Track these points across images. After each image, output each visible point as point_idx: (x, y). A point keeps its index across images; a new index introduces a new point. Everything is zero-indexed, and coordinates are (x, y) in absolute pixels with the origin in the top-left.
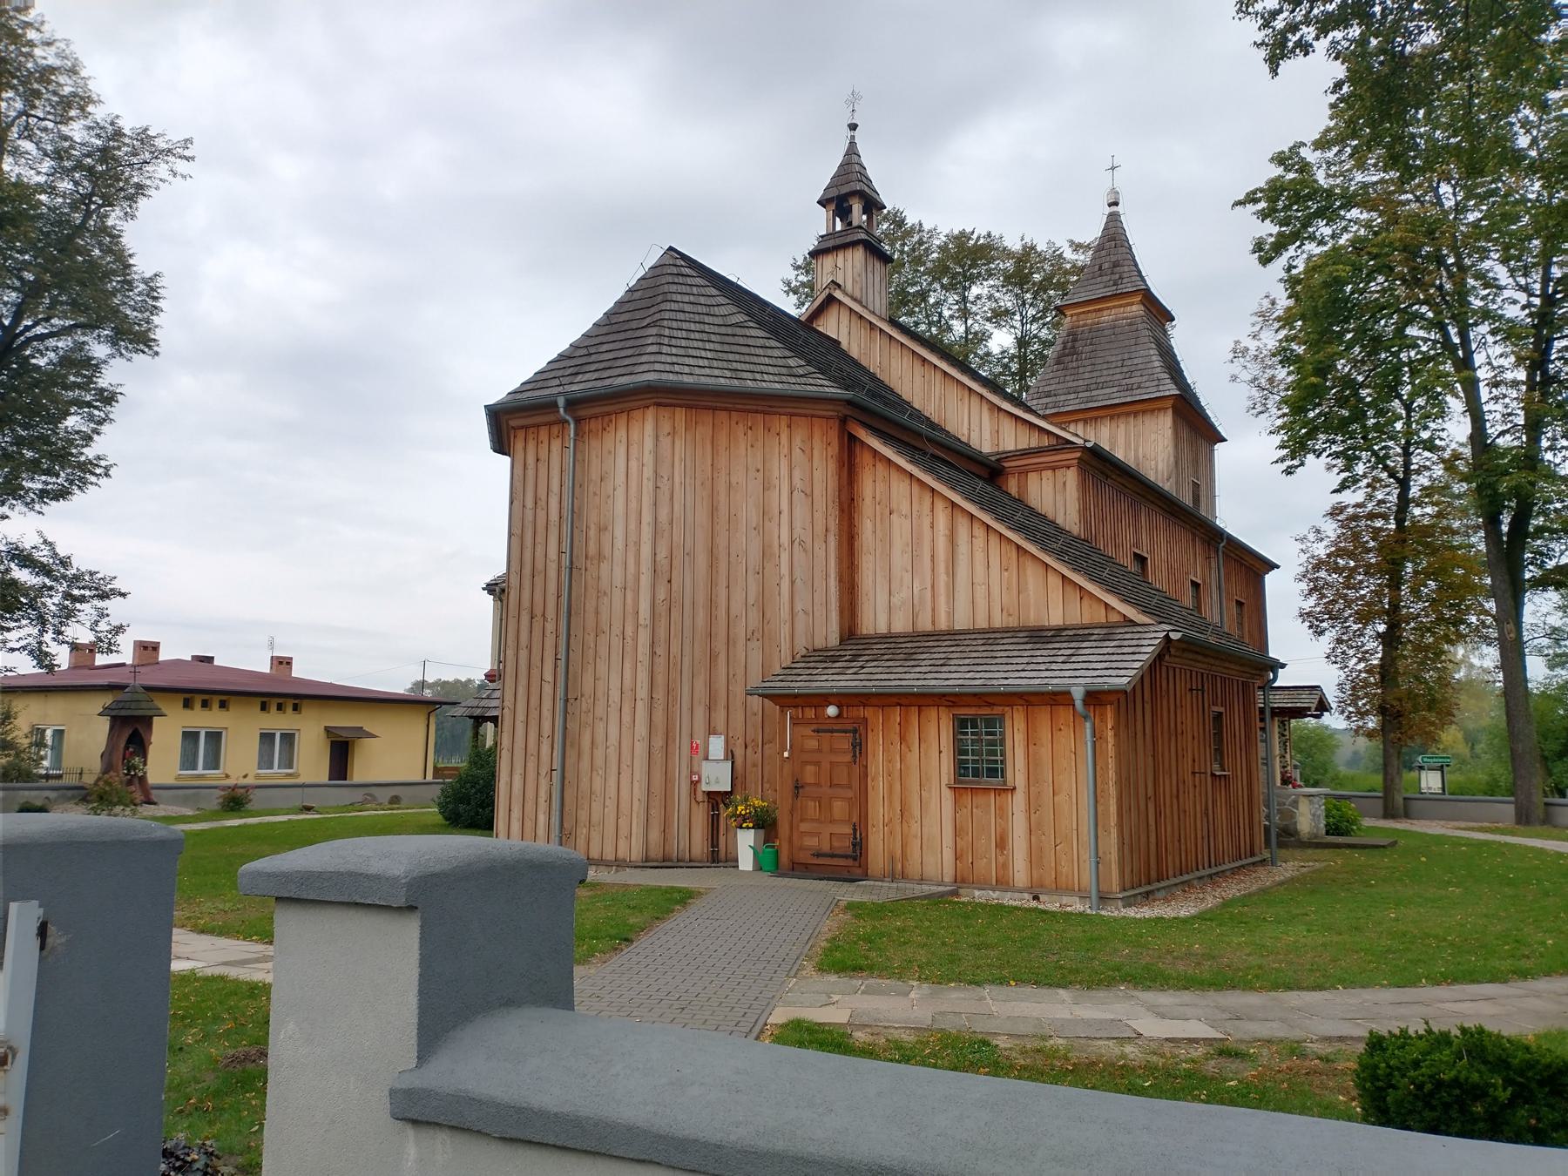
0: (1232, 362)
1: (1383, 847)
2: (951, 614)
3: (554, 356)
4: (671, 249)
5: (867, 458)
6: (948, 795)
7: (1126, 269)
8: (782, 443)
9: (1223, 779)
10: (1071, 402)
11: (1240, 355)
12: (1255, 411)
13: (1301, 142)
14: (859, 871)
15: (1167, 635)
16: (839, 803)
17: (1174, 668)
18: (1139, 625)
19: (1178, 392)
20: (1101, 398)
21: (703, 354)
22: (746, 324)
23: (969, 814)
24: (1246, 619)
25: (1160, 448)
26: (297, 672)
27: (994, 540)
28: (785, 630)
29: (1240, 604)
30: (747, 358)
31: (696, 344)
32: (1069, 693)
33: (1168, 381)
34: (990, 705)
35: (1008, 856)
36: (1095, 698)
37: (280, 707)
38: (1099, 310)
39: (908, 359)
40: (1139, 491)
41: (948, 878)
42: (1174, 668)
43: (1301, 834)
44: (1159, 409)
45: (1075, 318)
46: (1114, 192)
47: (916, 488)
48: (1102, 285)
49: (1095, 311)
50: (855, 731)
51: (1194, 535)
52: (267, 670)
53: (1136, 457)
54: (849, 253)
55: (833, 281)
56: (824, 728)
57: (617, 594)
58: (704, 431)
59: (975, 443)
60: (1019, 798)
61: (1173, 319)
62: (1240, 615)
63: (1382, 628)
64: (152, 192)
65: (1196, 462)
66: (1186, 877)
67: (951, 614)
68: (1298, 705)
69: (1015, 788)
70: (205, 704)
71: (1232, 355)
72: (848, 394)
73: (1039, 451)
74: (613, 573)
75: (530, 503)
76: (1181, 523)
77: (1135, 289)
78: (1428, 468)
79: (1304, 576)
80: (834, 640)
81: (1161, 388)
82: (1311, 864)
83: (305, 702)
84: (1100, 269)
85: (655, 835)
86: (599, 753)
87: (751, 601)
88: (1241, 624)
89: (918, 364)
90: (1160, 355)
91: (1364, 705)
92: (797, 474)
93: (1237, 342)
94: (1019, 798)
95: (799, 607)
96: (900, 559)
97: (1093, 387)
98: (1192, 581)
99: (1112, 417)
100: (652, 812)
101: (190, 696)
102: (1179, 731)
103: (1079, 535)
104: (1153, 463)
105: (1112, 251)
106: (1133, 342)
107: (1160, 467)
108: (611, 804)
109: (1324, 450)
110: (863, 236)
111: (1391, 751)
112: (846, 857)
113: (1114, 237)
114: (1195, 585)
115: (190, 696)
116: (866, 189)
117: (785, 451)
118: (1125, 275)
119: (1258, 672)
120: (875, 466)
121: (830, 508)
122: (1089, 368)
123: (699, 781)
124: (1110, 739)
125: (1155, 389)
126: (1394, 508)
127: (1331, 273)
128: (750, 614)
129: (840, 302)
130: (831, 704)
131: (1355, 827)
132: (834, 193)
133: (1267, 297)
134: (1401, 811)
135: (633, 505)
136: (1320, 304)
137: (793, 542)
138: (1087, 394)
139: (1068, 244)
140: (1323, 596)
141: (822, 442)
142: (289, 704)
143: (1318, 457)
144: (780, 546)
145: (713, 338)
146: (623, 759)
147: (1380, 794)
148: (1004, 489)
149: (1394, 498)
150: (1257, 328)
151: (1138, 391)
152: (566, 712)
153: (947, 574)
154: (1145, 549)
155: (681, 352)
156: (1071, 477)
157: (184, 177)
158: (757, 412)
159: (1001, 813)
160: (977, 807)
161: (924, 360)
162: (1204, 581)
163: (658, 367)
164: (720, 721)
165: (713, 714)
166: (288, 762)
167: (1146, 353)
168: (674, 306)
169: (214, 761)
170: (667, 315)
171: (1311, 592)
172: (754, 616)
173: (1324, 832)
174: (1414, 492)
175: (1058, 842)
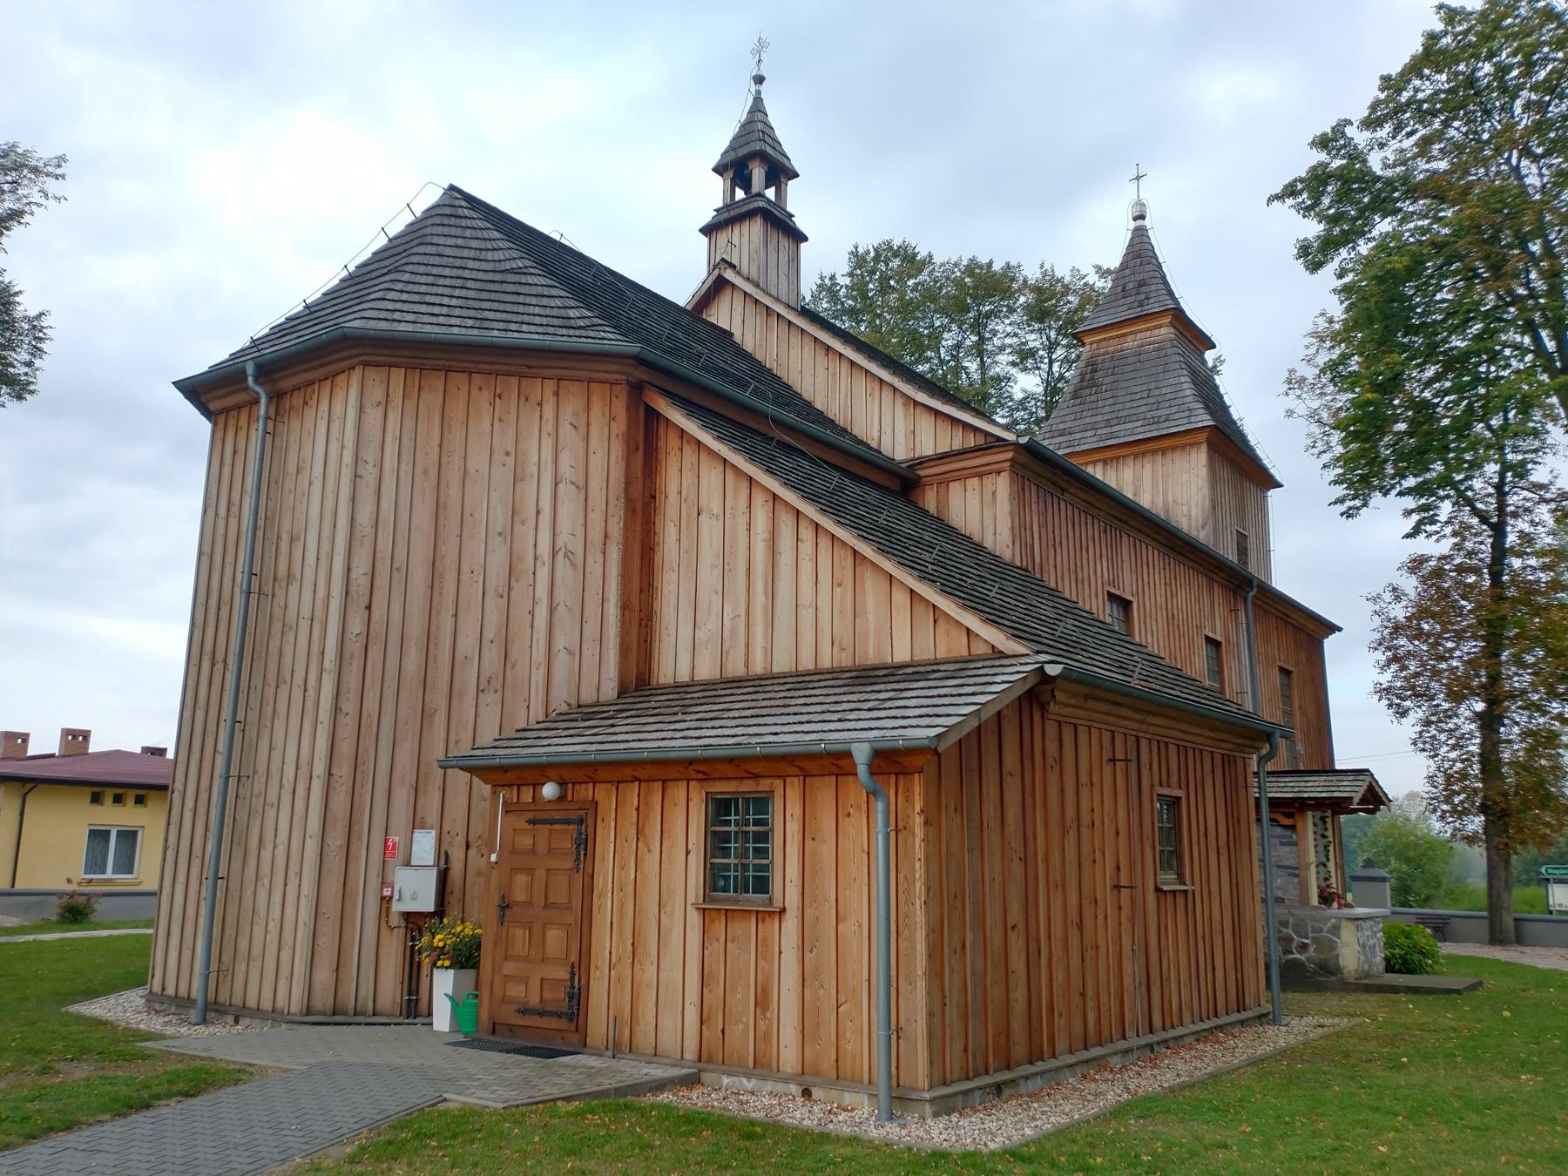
0: (1287, 394)
1: (1458, 992)
2: (769, 651)
4: (452, 188)
6: (694, 918)
9: (1180, 900)
10: (1089, 440)
11: (1296, 386)
12: (1315, 451)
13: (1345, 120)
14: (574, 1038)
15: (1041, 669)
16: (555, 932)
17: (1158, 742)
19: (1212, 423)
20: (1122, 433)
22: (524, 271)
25: (1194, 490)
28: (539, 676)
29: (1285, 672)
32: (848, 755)
33: (1202, 411)
34: (756, 777)
35: (771, 1020)
38: (1124, 335)
39: (809, 348)
40: (1118, 515)
41: (690, 1054)
42: (1138, 738)
43: (1345, 971)
44: (1192, 445)
45: (1095, 346)
46: (1140, 204)
47: (730, 476)
48: (1126, 308)
49: (1117, 336)
50: (581, 821)
51: (1211, 580)
53: (1165, 503)
54: (746, 226)
56: (540, 817)
57: (304, 625)
58: (432, 399)
59: (886, 449)
60: (791, 923)
62: (1287, 687)
63: (1480, 706)
64: (27, 218)
65: (1241, 509)
66: (1096, 1052)
67: (769, 651)
68: (1336, 794)
69: (783, 911)
70: (118, 799)
71: (1286, 386)
72: (635, 348)
74: (300, 601)
75: (223, 512)
76: (1189, 563)
77: (1163, 308)
78: (1527, 510)
79: (1380, 644)
80: (610, 690)
81: (1193, 419)
82: (1337, 1020)
85: (324, 976)
86: (266, 855)
87: (489, 634)
88: (1287, 698)
89: (821, 354)
90: (1194, 383)
91: (1462, 802)
93: (1292, 371)
94: (791, 923)
95: (560, 643)
96: (709, 577)
97: (1113, 423)
98: (1207, 638)
99: (1136, 456)
100: (321, 941)
102: (1085, 817)
103: (1013, 560)
104: (1185, 508)
106: (1160, 369)
107: (1193, 514)
108: (273, 927)
109: (1393, 487)
111: (1497, 859)
112: (559, 1015)
113: (1140, 252)
114: (1213, 643)
116: (769, 150)
117: (549, 427)
119: (1248, 742)
121: (611, 506)
122: (1110, 401)
124: (917, 830)
125: (1185, 421)
126: (1488, 560)
127: (1383, 266)
128: (486, 655)
130: (550, 780)
131: (1430, 962)
132: (732, 156)
133: (1323, 314)
134: (1513, 938)
135: (329, 503)
136: (1372, 304)
137: (554, 553)
139: (1094, 271)
140: (1404, 668)
142: (130, 796)
143: (1385, 495)
144: (536, 558)
145: (470, 284)
147: (1485, 914)
148: (921, 505)
149: (1487, 548)
150: (1313, 350)
151: (1166, 425)
153: (766, 594)
156: (1002, 485)
157: (58, 199)
159: (763, 949)
160: (732, 941)
161: (828, 348)
165: (421, 800)
166: (126, 863)
167: (1176, 381)
168: (429, 249)
171: (1389, 662)
172: (492, 656)
173: (1382, 967)
174: (1511, 539)
175: (842, 999)
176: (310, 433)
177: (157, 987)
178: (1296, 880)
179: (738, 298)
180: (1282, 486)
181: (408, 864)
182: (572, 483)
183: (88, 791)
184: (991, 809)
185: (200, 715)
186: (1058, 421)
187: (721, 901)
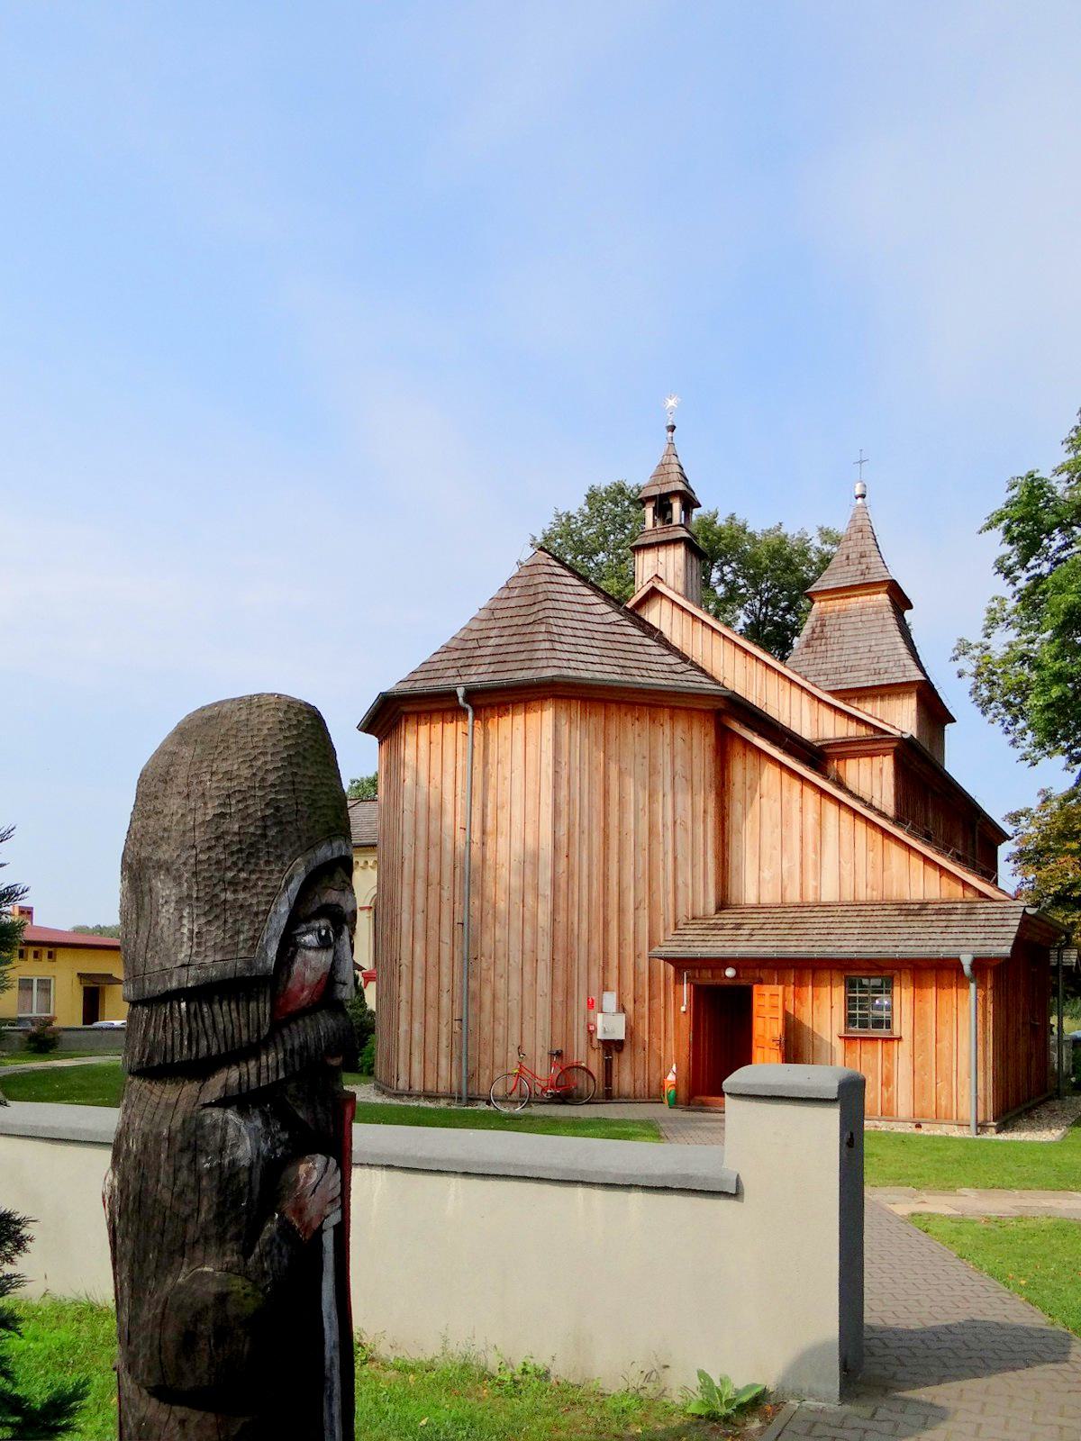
5: (738, 748)
7: (873, 559)
18: (995, 901)
23: (858, 1059)
30: (631, 656)
32: (958, 959)
36: (979, 964)
55: (656, 575)
59: (795, 728)
67: (818, 889)
73: (860, 742)
84: (848, 558)
86: (500, 1006)
89: (740, 654)
92: (679, 761)
117: (668, 740)
120: (745, 754)
129: (662, 595)
135: (531, 786)
137: (675, 822)
145: (596, 635)
146: (525, 1011)
155: (572, 648)
156: (887, 764)
159: (888, 1056)
163: (555, 662)
164: (613, 984)
170: (551, 613)
179: (666, 605)
180: (955, 721)
185: (420, 917)
187: (852, 1032)
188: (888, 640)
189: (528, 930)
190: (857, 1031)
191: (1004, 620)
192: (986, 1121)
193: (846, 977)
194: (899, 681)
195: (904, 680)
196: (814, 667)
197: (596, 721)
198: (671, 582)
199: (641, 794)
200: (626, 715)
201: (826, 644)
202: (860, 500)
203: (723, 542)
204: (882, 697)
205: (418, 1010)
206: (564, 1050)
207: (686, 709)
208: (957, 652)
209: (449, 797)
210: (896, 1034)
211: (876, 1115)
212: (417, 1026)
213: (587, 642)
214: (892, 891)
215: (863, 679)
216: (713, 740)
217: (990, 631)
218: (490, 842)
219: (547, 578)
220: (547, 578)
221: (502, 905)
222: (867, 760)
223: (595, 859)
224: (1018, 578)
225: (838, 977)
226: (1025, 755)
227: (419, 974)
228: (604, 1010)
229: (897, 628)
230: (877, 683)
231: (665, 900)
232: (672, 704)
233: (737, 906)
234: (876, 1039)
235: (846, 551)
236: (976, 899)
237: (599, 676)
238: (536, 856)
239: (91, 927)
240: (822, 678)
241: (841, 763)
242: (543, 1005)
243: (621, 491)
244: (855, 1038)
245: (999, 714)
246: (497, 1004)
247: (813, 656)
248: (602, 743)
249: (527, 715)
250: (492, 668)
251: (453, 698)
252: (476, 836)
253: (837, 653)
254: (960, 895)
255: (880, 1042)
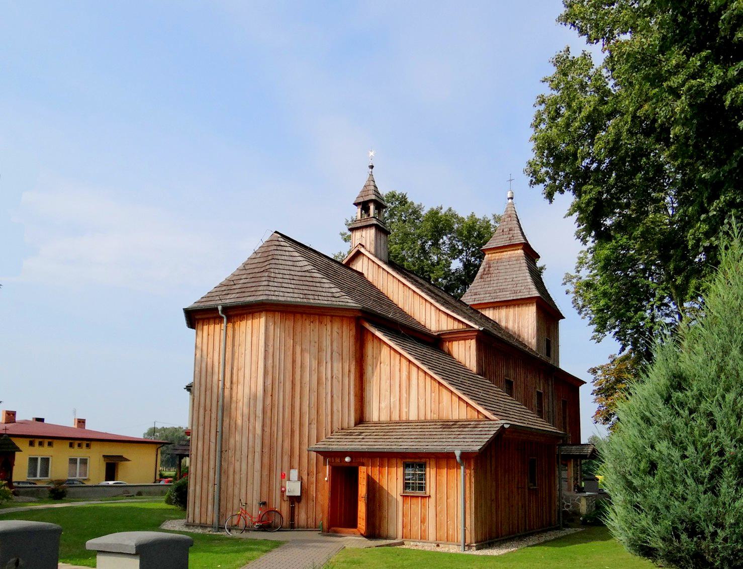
3: (217, 284)
7: (516, 232)
8: (328, 329)
19: (538, 295)
21: (290, 286)
22: (310, 271)
24: (567, 410)
26: (88, 426)
27: (428, 379)
30: (312, 288)
31: (286, 281)
32: (454, 452)
33: (534, 289)
35: (426, 526)
36: (465, 456)
37: (79, 445)
39: (396, 282)
48: (504, 240)
52: (73, 426)
55: (360, 244)
59: (428, 326)
61: (539, 257)
67: (408, 413)
69: (429, 497)
70: (41, 444)
83: (93, 443)
84: (503, 231)
86: (237, 477)
94: (432, 500)
96: (385, 385)
101: (32, 439)
104: (526, 330)
105: (509, 223)
107: (530, 332)
110: (375, 222)
115: (32, 439)
117: (329, 333)
118: (515, 235)
120: (373, 340)
123: (285, 490)
135: (254, 358)
137: (332, 377)
138: (495, 294)
141: (347, 328)
145: (295, 278)
151: (520, 294)
152: (221, 457)
154: (512, 377)
156: (473, 343)
158: (315, 314)
159: (423, 505)
160: (413, 504)
162: (544, 392)
164: (296, 465)
167: (524, 275)
169: (45, 472)
170: (273, 266)
175: (448, 520)
176: (243, 332)
177: (190, 520)
178: (566, 483)
179: (365, 259)
180: (564, 318)
181: (289, 480)
182: (337, 353)
183: (68, 442)
184: (488, 467)
185: (201, 428)
186: (474, 288)
188: (522, 275)
189: (251, 436)
190: (409, 492)
191: (586, 264)
192: (471, 543)
193: (404, 462)
194: (526, 297)
195: (529, 296)
196: (484, 289)
197: (289, 323)
198: (368, 247)
199: (313, 362)
200: (305, 320)
201: (490, 277)
202: (510, 200)
203: (442, 222)
204: (518, 305)
205: (199, 480)
206: (267, 502)
207: (340, 316)
208: (565, 280)
209: (216, 364)
210: (428, 494)
211: (418, 539)
212: (198, 488)
213: (289, 281)
214: (443, 414)
215: (508, 295)
216: (354, 334)
217: (579, 269)
218: (234, 387)
219: (275, 248)
220: (275, 248)
221: (239, 422)
222: (463, 342)
223: (287, 397)
224: (587, 241)
225: (400, 463)
226: (594, 336)
227: (200, 459)
228: (290, 480)
229: (527, 268)
230: (515, 298)
231: (325, 419)
232: (332, 314)
233: (369, 422)
234: (417, 497)
235: (502, 227)
236: (483, 419)
237: (289, 299)
238: (256, 396)
239: (597, 405)
240: (488, 295)
241: (450, 344)
242: (257, 475)
243: (394, 196)
244: (408, 496)
245: (587, 314)
246: (235, 476)
247: (483, 283)
248: (292, 334)
249: (253, 320)
250: (238, 295)
251: (216, 312)
252: (228, 384)
253: (496, 282)
254: (477, 417)
255: (420, 498)
